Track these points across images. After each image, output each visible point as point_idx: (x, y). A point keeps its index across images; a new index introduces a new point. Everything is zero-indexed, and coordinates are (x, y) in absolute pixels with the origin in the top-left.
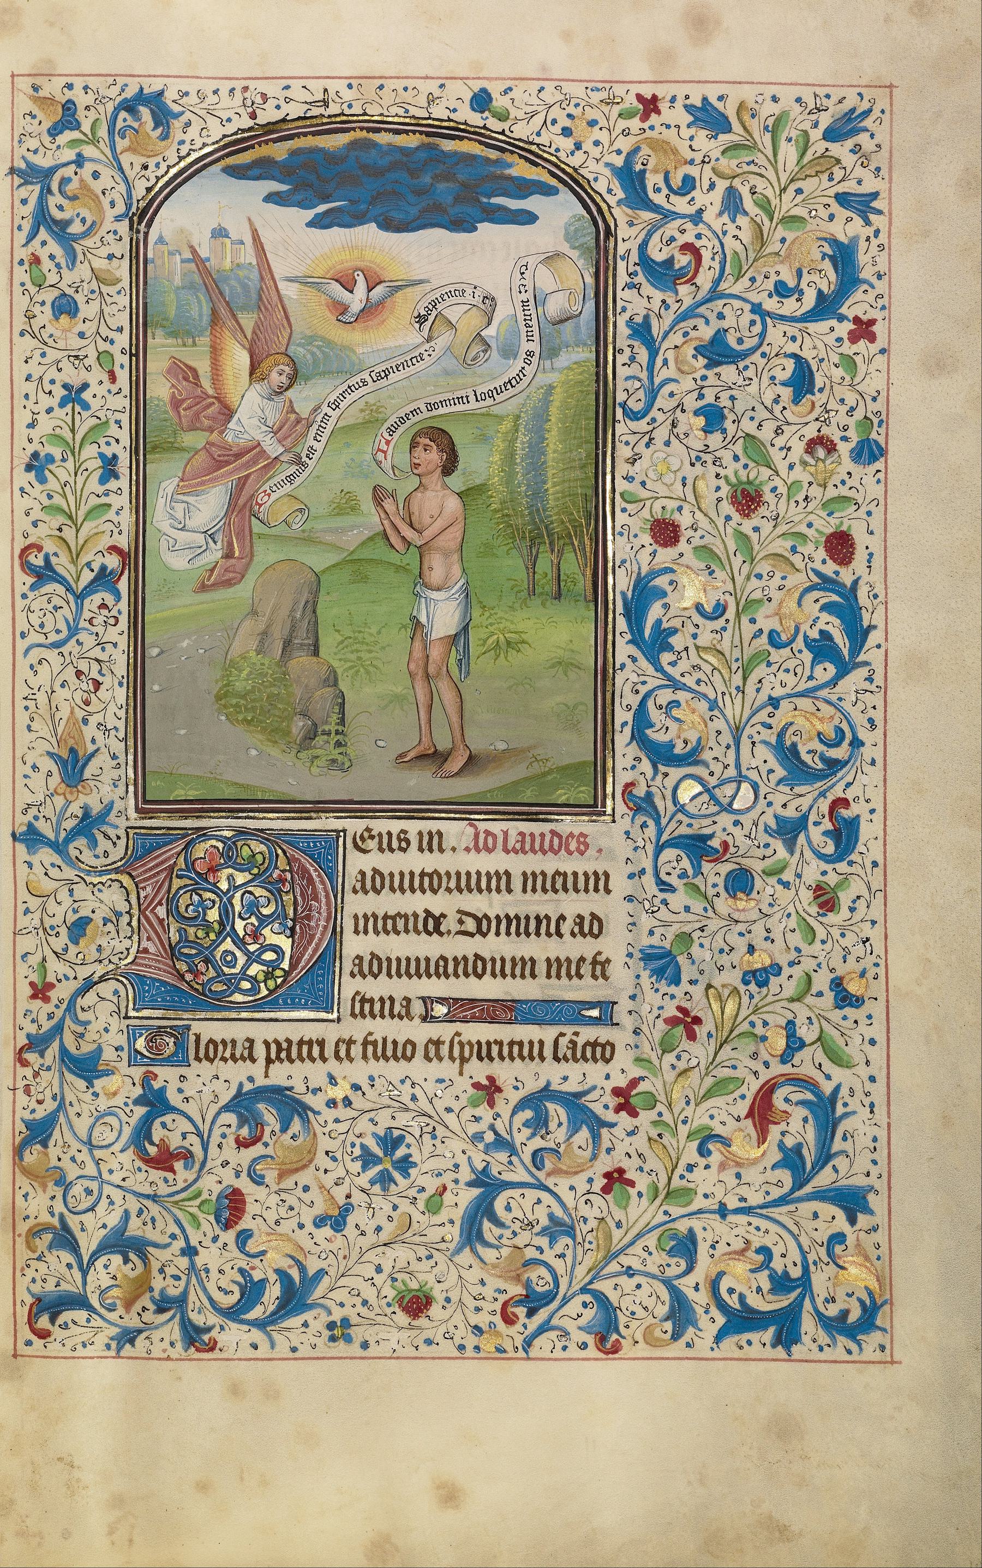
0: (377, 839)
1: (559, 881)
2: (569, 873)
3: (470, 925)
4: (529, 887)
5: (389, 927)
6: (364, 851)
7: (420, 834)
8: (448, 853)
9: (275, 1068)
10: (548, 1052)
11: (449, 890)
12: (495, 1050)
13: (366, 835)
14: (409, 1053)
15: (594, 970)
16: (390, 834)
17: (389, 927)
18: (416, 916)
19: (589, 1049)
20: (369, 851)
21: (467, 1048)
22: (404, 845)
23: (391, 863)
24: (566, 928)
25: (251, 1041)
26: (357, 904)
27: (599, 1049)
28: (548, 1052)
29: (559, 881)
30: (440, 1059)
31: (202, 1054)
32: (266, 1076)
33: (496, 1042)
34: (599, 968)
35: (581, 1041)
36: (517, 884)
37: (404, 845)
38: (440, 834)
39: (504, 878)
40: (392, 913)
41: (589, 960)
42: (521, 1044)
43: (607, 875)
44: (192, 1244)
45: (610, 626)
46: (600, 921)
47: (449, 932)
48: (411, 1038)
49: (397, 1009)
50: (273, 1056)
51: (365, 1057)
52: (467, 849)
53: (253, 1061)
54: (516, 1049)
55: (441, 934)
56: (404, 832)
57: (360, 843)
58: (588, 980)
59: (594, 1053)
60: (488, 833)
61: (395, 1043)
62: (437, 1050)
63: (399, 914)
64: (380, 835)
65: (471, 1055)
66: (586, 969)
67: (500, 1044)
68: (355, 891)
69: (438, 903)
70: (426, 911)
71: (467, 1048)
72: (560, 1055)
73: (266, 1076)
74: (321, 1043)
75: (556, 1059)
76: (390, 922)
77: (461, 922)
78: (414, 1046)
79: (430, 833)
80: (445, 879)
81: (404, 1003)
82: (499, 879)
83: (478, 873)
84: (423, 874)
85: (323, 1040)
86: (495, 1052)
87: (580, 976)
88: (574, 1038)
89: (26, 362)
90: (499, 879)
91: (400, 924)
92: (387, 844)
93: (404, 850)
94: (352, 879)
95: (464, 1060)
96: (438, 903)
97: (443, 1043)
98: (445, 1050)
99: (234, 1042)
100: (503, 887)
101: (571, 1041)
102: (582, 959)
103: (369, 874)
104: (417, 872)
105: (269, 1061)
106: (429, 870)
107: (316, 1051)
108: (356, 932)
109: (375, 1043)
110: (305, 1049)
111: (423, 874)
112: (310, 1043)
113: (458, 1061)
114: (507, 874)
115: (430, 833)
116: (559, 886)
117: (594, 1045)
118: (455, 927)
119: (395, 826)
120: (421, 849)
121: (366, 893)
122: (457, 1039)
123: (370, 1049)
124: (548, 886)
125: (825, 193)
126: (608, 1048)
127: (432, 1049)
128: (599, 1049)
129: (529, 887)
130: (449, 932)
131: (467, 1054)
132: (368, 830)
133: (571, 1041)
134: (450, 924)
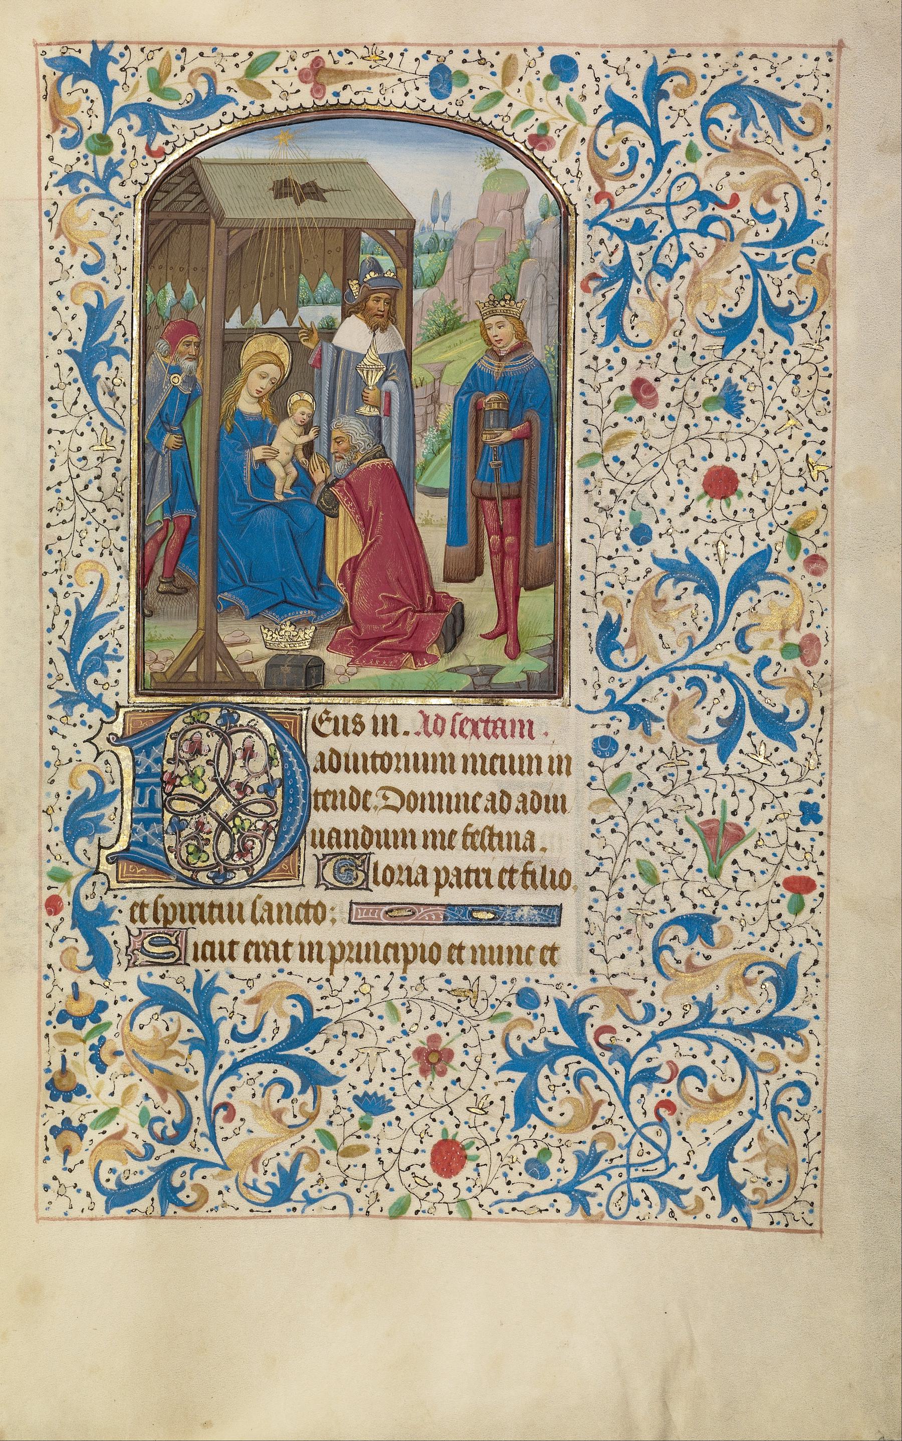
0: (333, 722)
1: (497, 764)
3: (394, 800)
4: (470, 768)
7: (375, 718)
8: (401, 736)
9: (445, 891)
11: (398, 770)
13: (324, 717)
14: (565, 883)
16: (345, 718)
18: (343, 793)
21: (171, 912)
22: (358, 728)
23: (343, 744)
24: (481, 804)
26: (321, 782)
29: (497, 764)
31: (380, 879)
32: (437, 894)
33: (198, 904)
34: (469, 839)
36: (420, 841)
37: (358, 728)
38: (394, 717)
43: (569, 758)
52: (418, 734)
53: (425, 883)
55: (366, 809)
57: (318, 725)
59: (307, 914)
61: (553, 873)
64: (336, 719)
67: (201, 906)
68: (316, 770)
71: (171, 912)
72: (258, 917)
73: (437, 894)
74: (488, 872)
75: (254, 921)
77: (385, 798)
80: (395, 760)
83: (425, 755)
84: (374, 756)
85: (489, 870)
92: (341, 727)
94: (313, 761)
95: (407, 961)
97: (147, 906)
99: (409, 869)
102: (453, 833)
103: (327, 755)
105: (439, 886)
107: (483, 877)
109: (533, 873)
110: (473, 876)
112: (477, 871)
115: (384, 718)
116: (497, 767)
117: (307, 906)
120: (375, 733)
122: (160, 902)
123: (529, 877)
124: (487, 768)
128: (311, 911)
129: (470, 768)
131: (411, 957)
132: (326, 712)
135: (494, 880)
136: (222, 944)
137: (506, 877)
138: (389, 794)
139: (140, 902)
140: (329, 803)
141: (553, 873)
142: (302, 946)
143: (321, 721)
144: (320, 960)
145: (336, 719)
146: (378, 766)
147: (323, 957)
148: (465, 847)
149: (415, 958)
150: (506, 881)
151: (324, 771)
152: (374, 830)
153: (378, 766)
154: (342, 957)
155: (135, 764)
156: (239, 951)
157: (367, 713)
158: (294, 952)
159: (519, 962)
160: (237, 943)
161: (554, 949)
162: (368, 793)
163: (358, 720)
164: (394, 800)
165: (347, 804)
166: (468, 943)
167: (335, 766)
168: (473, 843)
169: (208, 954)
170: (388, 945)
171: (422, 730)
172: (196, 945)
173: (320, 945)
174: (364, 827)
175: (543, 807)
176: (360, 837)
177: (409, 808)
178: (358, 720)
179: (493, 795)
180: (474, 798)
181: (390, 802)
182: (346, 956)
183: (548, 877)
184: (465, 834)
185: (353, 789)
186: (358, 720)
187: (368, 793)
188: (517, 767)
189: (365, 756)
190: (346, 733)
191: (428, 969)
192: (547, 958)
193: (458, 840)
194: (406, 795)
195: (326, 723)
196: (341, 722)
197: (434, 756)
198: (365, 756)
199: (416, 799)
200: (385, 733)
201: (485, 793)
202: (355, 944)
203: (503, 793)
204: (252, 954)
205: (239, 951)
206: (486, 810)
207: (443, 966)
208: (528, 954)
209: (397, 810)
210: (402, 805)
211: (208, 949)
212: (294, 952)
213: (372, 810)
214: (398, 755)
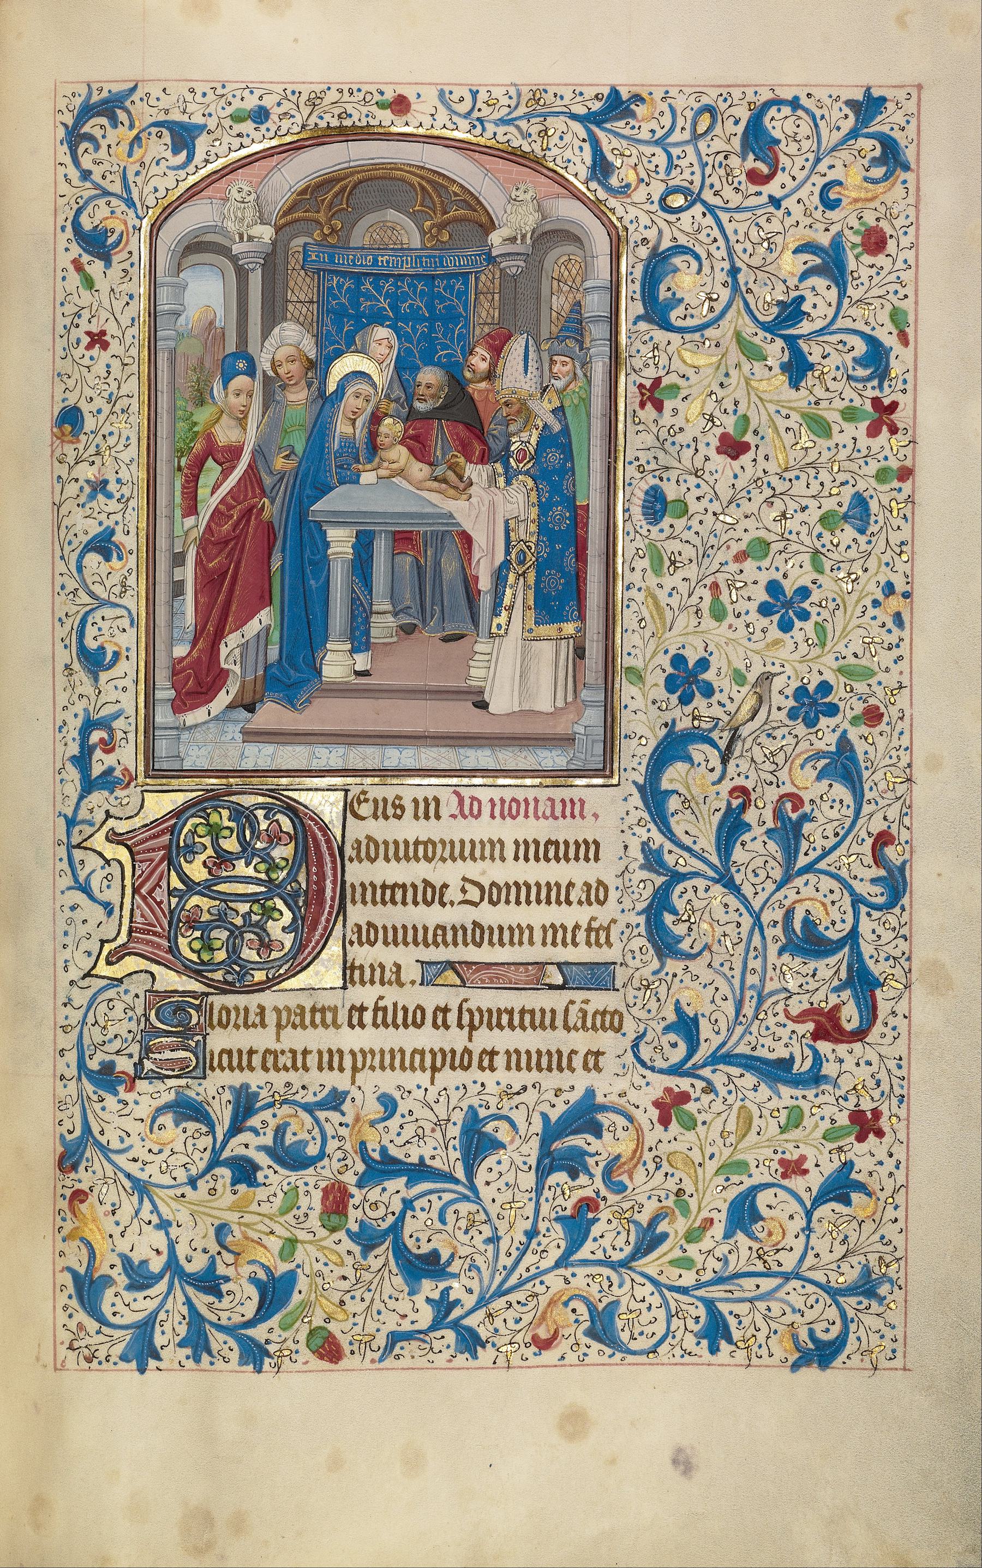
2: (561, 841)
3: (474, 894)
5: (388, 897)
6: (363, 819)
7: (416, 801)
9: (288, 1032)
10: (559, 1022)
13: (362, 797)
15: (588, 936)
16: (385, 800)
17: (388, 897)
18: (414, 887)
22: (399, 812)
25: (262, 1009)
27: (608, 1018)
28: (559, 1022)
32: (278, 1040)
33: (506, 1010)
34: (593, 934)
35: (590, 1009)
36: (510, 852)
37: (399, 812)
38: (437, 800)
39: (498, 846)
40: (390, 882)
41: (585, 926)
42: (532, 1012)
44: (165, 1217)
48: (420, 1003)
49: (388, 974)
51: (375, 1025)
54: (527, 1018)
55: (443, 904)
57: (356, 805)
58: (583, 947)
60: (473, 799)
61: (405, 1010)
62: (491, 1061)
63: (396, 885)
66: (581, 936)
67: (510, 1012)
68: (351, 860)
70: (425, 881)
73: (278, 1040)
74: (335, 1010)
75: (567, 1028)
76: (388, 892)
77: (464, 891)
79: (426, 800)
81: (394, 969)
86: (505, 1020)
88: (584, 1006)
89: (625, 799)
93: (399, 817)
95: (472, 1027)
98: (452, 1018)
99: (246, 1010)
101: (581, 1010)
102: (577, 927)
105: (279, 1026)
107: (329, 1016)
109: (385, 1009)
111: (417, 843)
112: (323, 1010)
113: (467, 1029)
114: (501, 842)
115: (426, 800)
116: (551, 854)
118: (460, 897)
120: (416, 817)
121: (360, 861)
122: (465, 1006)
123: (380, 1014)
125: (870, 1241)
126: (616, 1018)
128: (608, 1018)
133: (581, 1010)
134: (453, 894)
138: (468, 886)
139: (489, 1049)
141: (405, 1010)
142: (320, 1053)
143: (359, 803)
144: (341, 1069)
145: (376, 801)
149: (443, 1065)
150: (486, 1063)
154: (364, 1066)
156: (257, 1060)
158: (312, 1060)
160: (256, 1052)
161: (598, 1054)
162: (445, 886)
164: (474, 894)
165: (420, 898)
166: (501, 1048)
167: (373, 855)
170: (415, 1051)
171: (457, 812)
173: (340, 1052)
176: (469, 932)
177: (491, 902)
181: (468, 897)
183: (400, 1014)
184: (589, 929)
186: (397, 802)
187: (445, 886)
188: (467, 852)
190: (386, 818)
191: (459, 1077)
192: (355, 1021)
193: (581, 936)
196: (381, 805)
197: (526, 842)
198: (406, 843)
199: (499, 890)
200: (427, 817)
201: (579, 884)
202: (377, 1050)
204: (270, 1064)
207: (475, 1073)
208: (570, 1060)
209: (476, 905)
210: (482, 899)
212: (312, 1060)
213: (448, 906)
214: (443, 842)
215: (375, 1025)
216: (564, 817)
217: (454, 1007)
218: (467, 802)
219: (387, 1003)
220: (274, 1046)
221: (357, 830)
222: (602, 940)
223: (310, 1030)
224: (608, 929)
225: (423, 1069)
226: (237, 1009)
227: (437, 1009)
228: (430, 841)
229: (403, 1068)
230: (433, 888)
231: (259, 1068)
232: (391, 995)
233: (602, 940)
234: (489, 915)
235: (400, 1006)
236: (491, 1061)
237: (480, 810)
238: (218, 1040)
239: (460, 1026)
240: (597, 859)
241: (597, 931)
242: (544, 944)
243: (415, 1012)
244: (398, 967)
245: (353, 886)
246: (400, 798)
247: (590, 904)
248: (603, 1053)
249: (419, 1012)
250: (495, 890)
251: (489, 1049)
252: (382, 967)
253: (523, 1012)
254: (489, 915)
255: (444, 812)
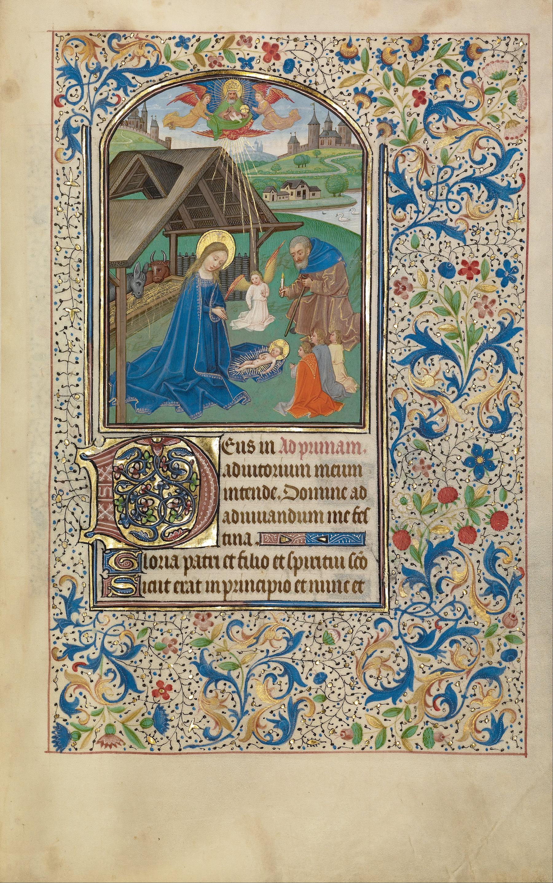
0: (235, 446)
1: (336, 471)
10: (346, 563)
12: (315, 562)
14: (265, 564)
16: (243, 443)
18: (258, 489)
19: (358, 561)
20: (231, 454)
22: (251, 449)
23: (244, 460)
24: (348, 494)
26: (227, 483)
28: (346, 563)
30: (282, 567)
32: (185, 574)
34: (357, 516)
36: (313, 472)
37: (251, 449)
38: (272, 443)
42: (330, 559)
45: (86, 265)
46: (365, 490)
47: (279, 498)
50: (189, 565)
53: (177, 566)
54: (328, 562)
55: (273, 498)
56: (251, 441)
60: (291, 441)
62: (281, 562)
63: (249, 489)
65: (301, 564)
66: (350, 518)
67: (318, 559)
68: (224, 475)
69: (270, 482)
73: (185, 574)
74: (217, 558)
76: (244, 493)
77: (285, 492)
78: (268, 559)
82: (355, 470)
87: (346, 521)
90: (355, 470)
91: (250, 494)
94: (223, 470)
96: (270, 482)
98: (285, 563)
99: (167, 558)
100: (357, 473)
102: (348, 512)
103: (232, 466)
104: (258, 466)
105: (186, 568)
106: (264, 464)
108: (226, 499)
109: (246, 558)
112: (210, 558)
118: (283, 495)
119: (246, 438)
120: (261, 452)
121: (343, 453)
122: (292, 556)
123: (243, 561)
127: (228, 561)
130: (279, 498)
131: (299, 565)
132: (230, 439)
134: (279, 493)
135: (221, 564)
136: (160, 583)
137: (278, 562)
138: (287, 489)
140: (250, 495)
142: (207, 583)
143: (227, 445)
144: (218, 591)
145: (238, 444)
146: (263, 473)
147: (234, 565)
148: (354, 521)
150: (299, 588)
151: (229, 476)
152: (296, 511)
153: (263, 473)
155: (98, 475)
156: (171, 587)
157: (277, 439)
159: (253, 590)
160: (170, 582)
161: (361, 583)
163: (251, 444)
164: (292, 493)
165: (261, 495)
168: (359, 518)
169: (152, 589)
172: (145, 583)
174: (290, 510)
175: (330, 469)
178: (251, 444)
179: (356, 489)
180: (343, 491)
181: (288, 495)
182: (158, 565)
184: (355, 513)
185: (265, 487)
186: (251, 444)
187: (275, 488)
189: (255, 467)
190: (244, 452)
192: (357, 589)
193: (350, 518)
194: (271, 489)
195: (230, 446)
197: (297, 467)
203: (362, 488)
204: (179, 589)
205: (171, 587)
206: (352, 498)
209: (293, 499)
211: (152, 586)
213: (277, 499)
215: (240, 566)
216: (348, 452)
217: (286, 556)
218: (288, 443)
219: (247, 554)
220: (183, 579)
221: (226, 460)
222: (362, 519)
223: (203, 569)
224: (365, 513)
225: (264, 591)
226: (161, 558)
227: (276, 558)
228: (268, 465)
229: (317, 591)
230: (268, 490)
231: (308, 591)
232: (249, 551)
233: (362, 519)
234: (299, 506)
235: (254, 557)
236: (281, 562)
237: (295, 449)
238: (149, 576)
239: (289, 567)
240: (360, 475)
241: (359, 514)
242: (329, 521)
243: (262, 560)
244: (249, 535)
245: (225, 490)
246: (252, 442)
247: (357, 499)
248: (364, 583)
249: (153, 560)
250: (303, 492)
251: (359, 580)
252: (240, 536)
253: (325, 558)
254: (299, 506)
255: (277, 448)
